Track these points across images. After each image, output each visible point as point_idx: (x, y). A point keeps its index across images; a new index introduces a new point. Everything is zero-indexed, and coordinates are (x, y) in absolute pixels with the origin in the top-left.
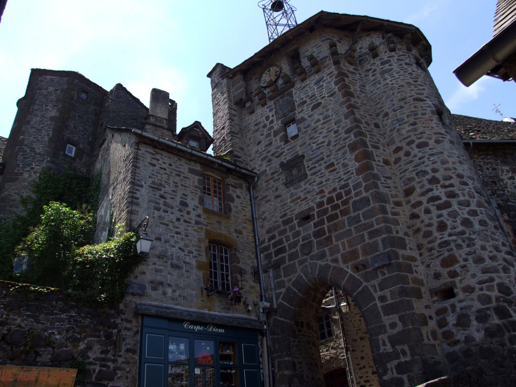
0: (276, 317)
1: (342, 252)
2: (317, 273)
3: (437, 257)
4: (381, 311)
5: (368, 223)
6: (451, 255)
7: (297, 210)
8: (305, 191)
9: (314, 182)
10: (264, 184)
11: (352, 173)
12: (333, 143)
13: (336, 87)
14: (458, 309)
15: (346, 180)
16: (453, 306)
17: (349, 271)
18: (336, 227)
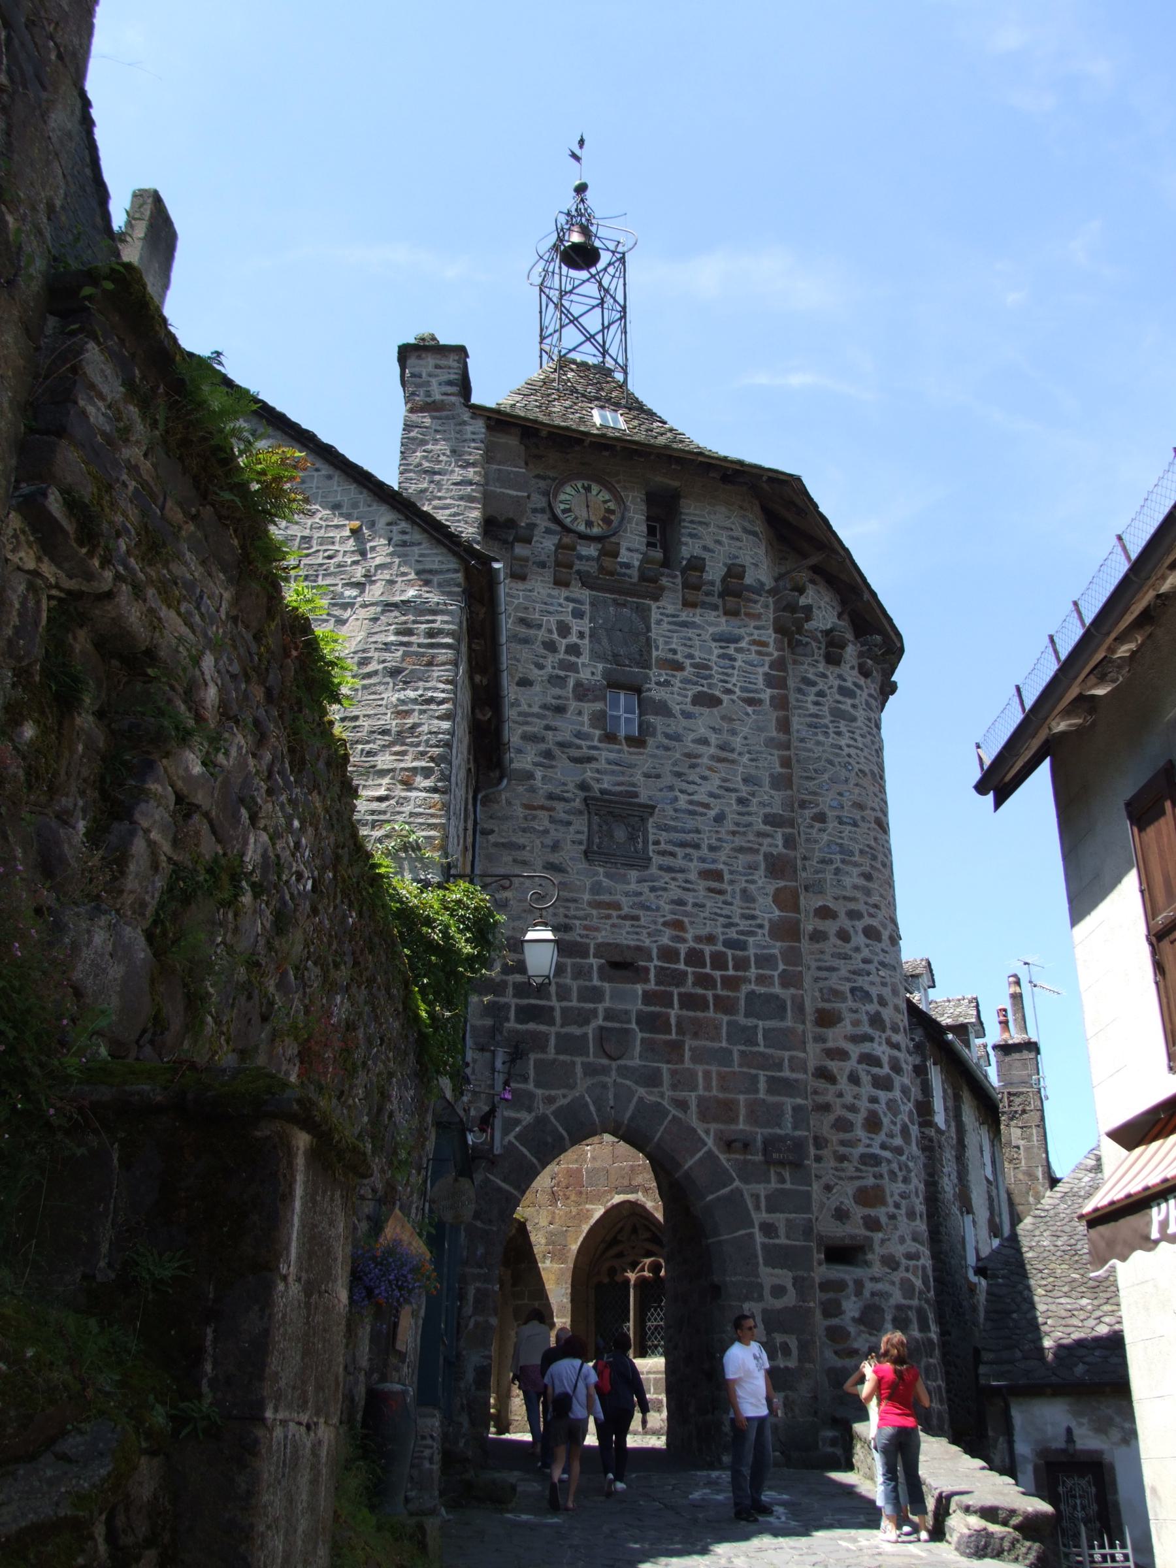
0: (492, 1178)
1: (701, 1092)
2: (628, 1114)
3: (852, 1178)
4: (760, 1252)
5: (772, 1056)
6: (878, 1186)
7: (603, 933)
8: (636, 899)
9: (665, 889)
10: (520, 812)
11: (761, 926)
12: (729, 825)
13: (769, 691)
14: (867, 1293)
15: (742, 933)
16: (859, 1284)
17: (710, 1142)
18: (698, 1029)
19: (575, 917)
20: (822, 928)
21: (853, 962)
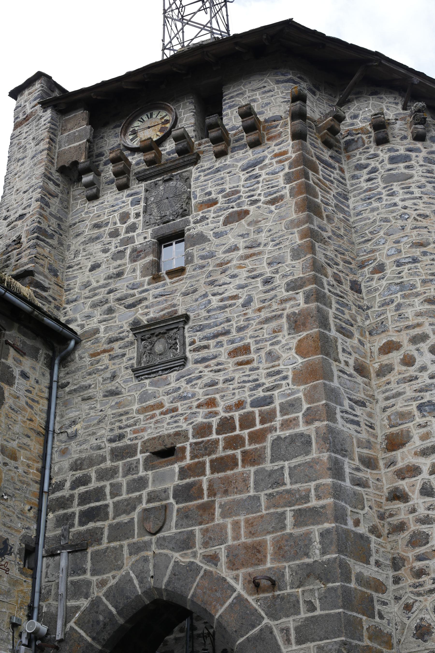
1: (230, 542)
2: (166, 580)
7: (149, 431)
9: (200, 377)
11: (285, 378)
12: (256, 304)
15: (268, 390)
17: (239, 587)
19: (128, 426)
20: (387, 362)
21: (419, 381)
